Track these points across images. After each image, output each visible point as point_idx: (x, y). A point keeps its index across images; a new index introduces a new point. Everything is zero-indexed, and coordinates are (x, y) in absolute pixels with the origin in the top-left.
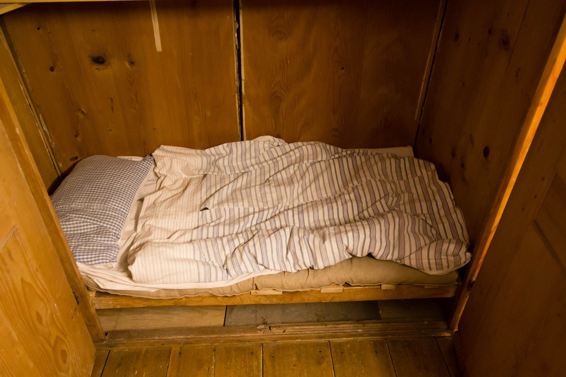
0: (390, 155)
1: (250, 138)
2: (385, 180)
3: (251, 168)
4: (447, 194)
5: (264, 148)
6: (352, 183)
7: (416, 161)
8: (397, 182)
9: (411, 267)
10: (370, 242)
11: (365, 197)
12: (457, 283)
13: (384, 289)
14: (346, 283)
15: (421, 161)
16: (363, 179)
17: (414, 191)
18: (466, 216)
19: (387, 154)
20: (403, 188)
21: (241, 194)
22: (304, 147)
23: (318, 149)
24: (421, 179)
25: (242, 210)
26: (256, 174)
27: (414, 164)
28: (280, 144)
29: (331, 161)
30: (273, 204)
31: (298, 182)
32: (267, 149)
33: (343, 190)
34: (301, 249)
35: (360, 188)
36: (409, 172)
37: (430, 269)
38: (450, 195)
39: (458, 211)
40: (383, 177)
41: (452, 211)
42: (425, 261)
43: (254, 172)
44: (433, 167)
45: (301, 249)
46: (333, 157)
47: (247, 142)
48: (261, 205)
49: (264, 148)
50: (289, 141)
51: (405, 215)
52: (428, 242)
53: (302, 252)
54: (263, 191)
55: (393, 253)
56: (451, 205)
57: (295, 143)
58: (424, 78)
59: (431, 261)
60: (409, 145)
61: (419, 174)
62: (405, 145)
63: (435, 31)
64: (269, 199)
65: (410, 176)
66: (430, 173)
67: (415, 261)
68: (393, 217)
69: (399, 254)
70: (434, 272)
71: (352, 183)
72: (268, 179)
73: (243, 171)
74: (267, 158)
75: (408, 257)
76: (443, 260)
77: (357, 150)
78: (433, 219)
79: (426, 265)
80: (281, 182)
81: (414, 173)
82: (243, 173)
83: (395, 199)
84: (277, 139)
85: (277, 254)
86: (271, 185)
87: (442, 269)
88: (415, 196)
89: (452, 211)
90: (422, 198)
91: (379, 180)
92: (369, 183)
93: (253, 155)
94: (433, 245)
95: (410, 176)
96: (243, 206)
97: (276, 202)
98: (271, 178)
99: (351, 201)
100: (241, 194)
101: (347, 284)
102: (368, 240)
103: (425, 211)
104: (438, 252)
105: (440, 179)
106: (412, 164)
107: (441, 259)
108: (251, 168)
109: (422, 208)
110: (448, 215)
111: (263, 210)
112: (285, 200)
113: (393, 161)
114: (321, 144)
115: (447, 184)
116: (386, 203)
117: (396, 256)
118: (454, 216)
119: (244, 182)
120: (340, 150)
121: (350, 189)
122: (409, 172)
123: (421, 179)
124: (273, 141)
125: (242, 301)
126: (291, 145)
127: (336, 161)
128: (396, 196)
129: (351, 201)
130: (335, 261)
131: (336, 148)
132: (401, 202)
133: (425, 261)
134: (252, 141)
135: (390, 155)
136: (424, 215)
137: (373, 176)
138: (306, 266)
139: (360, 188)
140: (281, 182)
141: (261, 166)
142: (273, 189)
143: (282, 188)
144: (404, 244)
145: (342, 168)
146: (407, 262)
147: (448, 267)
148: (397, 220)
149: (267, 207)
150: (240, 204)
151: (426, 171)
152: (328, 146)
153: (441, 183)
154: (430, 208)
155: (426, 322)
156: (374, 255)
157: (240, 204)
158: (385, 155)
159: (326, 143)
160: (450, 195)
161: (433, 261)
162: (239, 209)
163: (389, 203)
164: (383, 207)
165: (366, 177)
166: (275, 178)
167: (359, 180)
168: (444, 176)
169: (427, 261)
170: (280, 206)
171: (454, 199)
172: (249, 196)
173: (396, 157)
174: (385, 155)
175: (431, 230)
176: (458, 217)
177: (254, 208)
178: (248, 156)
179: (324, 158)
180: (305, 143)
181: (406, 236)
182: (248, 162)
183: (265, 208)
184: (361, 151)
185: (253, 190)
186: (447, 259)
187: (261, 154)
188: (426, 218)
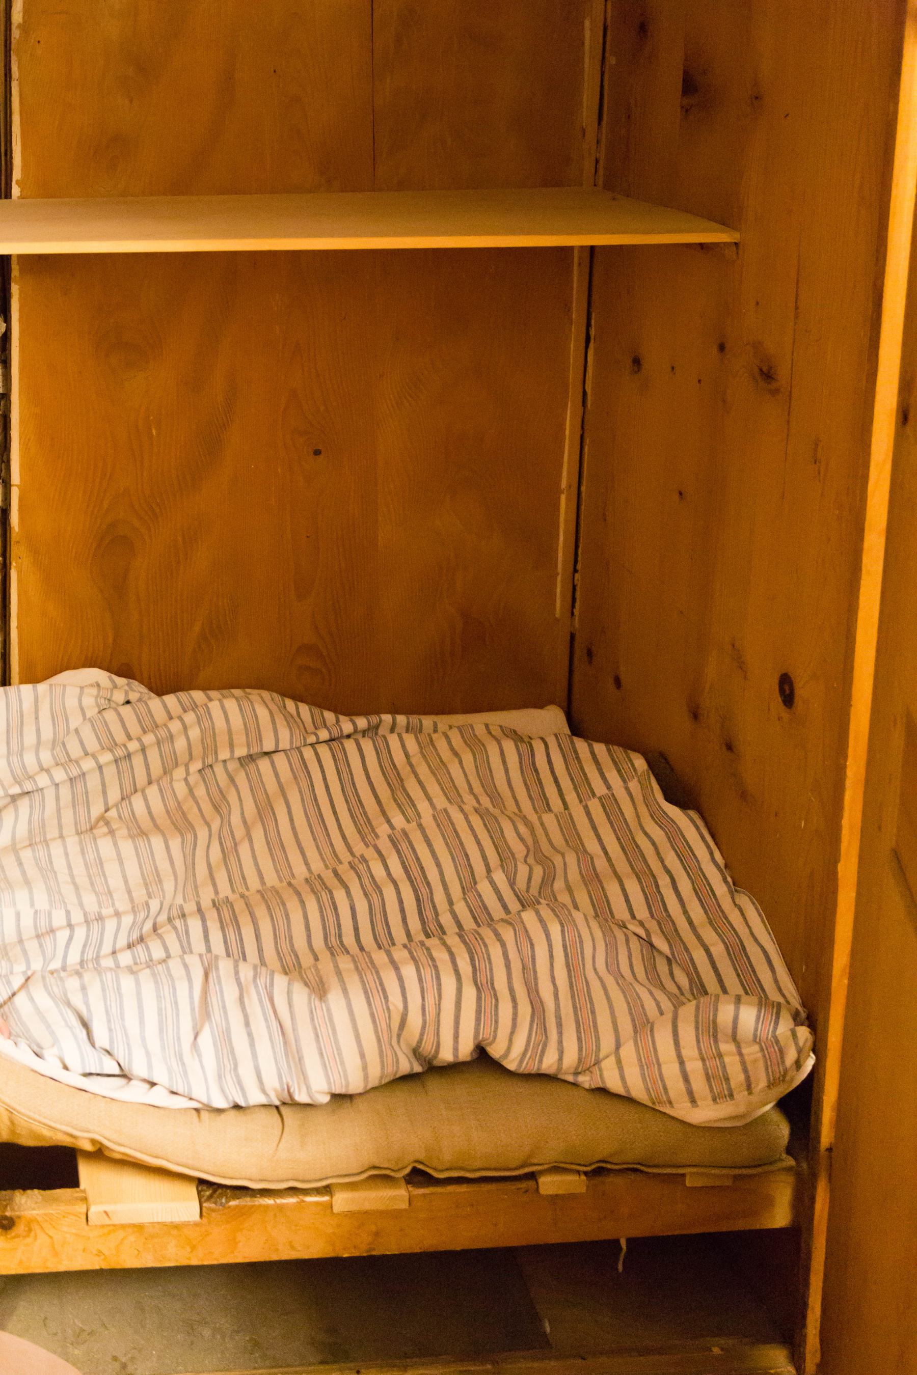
0: (496, 731)
1: (32, 677)
2: (496, 811)
3: (43, 780)
4: (701, 852)
5: (82, 709)
6: (389, 821)
7: (581, 745)
8: (533, 817)
9: (628, 1100)
10: (479, 999)
11: (438, 865)
12: (791, 1162)
13: (551, 1192)
14: (415, 1171)
15: (600, 748)
16: (423, 806)
17: (592, 846)
18: (771, 915)
19: (487, 726)
20: (557, 838)
21: (20, 864)
22: (215, 706)
23: (263, 713)
24: (610, 805)
25: (27, 921)
26: (58, 799)
27: (578, 758)
28: (133, 697)
29: (308, 753)
30: (132, 900)
31: (208, 825)
32: (92, 712)
33: (359, 848)
34: (247, 1024)
35: (416, 837)
36: (566, 783)
37: (693, 1101)
38: (711, 854)
39: (744, 900)
40: (486, 802)
41: (726, 903)
42: (671, 1070)
43: (50, 794)
44: (640, 763)
45: (247, 1024)
46: (312, 739)
47: (27, 688)
48: (90, 902)
49: (82, 709)
50: (160, 691)
51: (578, 916)
52: (666, 1005)
53: (250, 1034)
54: (91, 856)
55: (560, 1042)
56: (721, 890)
57: (182, 695)
58: (564, 484)
59: (689, 1066)
60: (551, 702)
61: (600, 788)
62: (539, 705)
63: (574, 346)
64: (115, 882)
65: (571, 797)
66: (633, 785)
67: (637, 1070)
68: (541, 920)
69: (580, 1049)
70: (705, 1113)
71: (389, 821)
72: (102, 818)
73: (16, 790)
74: (92, 744)
75: (612, 1059)
76: (727, 1060)
77: (387, 718)
78: (672, 935)
79: (676, 1087)
80: (146, 823)
81: (581, 784)
82: (14, 798)
83: (538, 871)
84: (121, 681)
85: (161, 1030)
86: (118, 834)
87: (731, 1095)
88: (601, 864)
89: (726, 903)
90: (622, 866)
91: (476, 810)
92: (443, 820)
93: (47, 733)
94: (687, 1011)
95: (571, 797)
96: (32, 905)
97: (140, 894)
98: (113, 813)
99: (395, 883)
100: (20, 864)
101: (418, 1176)
102: (470, 993)
103: (642, 912)
104: (710, 1030)
105: (668, 799)
106: (572, 758)
107: (720, 1055)
108: (43, 780)
109: (627, 896)
110: (717, 918)
111: (100, 918)
112: (169, 885)
113: (509, 746)
114: (266, 694)
115: (692, 813)
116: (512, 884)
117: (571, 1058)
118: (734, 917)
119: (22, 829)
120: (329, 716)
121: (384, 844)
122: (566, 783)
123: (610, 805)
124: (109, 684)
125: (56, 1254)
126: (170, 699)
127: (324, 750)
128: (539, 862)
129: (395, 883)
130: (366, 1077)
131: (316, 711)
132: (559, 884)
133: (671, 1070)
134: (42, 687)
135: (496, 731)
136: (641, 924)
137: (452, 793)
138: (264, 1092)
139: (416, 837)
140: (146, 823)
141: (75, 772)
142: (127, 847)
143: (157, 842)
144: (593, 1012)
145: (345, 776)
146: (614, 1084)
147: (749, 1087)
148: (555, 929)
149: (111, 911)
150: (22, 896)
151: (623, 780)
152: (290, 704)
153: (673, 811)
154: (654, 898)
155: (716, 1350)
156: (496, 1051)
157: (22, 896)
158: (480, 730)
159: (284, 694)
160: (711, 854)
161: (694, 1066)
162: (18, 915)
163: (521, 883)
164: (500, 898)
165: (429, 799)
166: (126, 813)
167: (410, 812)
168: (680, 793)
169: (677, 1066)
170: (155, 905)
171: (726, 866)
172: (48, 871)
173: (516, 736)
174: (480, 730)
175: (671, 974)
176: (751, 921)
177: (68, 912)
178: (30, 738)
179: (284, 744)
180: (214, 694)
181: (595, 984)
182: (30, 759)
183: (105, 912)
184: (401, 719)
185: (56, 849)
186: (741, 1054)
187: (73, 733)
188: (647, 931)
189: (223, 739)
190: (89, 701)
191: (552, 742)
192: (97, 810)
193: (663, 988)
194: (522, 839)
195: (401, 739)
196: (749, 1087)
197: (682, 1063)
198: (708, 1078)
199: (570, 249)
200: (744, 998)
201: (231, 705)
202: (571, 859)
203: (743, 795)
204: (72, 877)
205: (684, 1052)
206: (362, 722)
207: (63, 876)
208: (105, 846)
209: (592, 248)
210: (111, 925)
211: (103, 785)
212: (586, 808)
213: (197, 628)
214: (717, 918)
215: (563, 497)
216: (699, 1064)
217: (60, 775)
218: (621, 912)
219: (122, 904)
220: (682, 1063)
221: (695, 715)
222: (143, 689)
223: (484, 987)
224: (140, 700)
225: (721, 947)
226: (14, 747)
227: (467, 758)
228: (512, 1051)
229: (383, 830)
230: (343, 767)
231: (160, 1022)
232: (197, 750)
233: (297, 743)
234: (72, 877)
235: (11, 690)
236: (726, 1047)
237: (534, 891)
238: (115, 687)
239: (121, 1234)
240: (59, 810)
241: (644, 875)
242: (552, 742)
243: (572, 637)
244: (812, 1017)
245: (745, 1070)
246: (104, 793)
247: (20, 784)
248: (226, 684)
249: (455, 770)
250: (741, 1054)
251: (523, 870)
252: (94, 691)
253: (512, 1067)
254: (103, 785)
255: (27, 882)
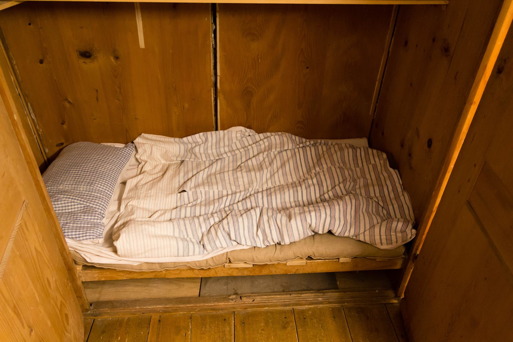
0: (348, 145)
1: (223, 129)
3: (225, 156)
7: (370, 150)
8: (354, 169)
10: (331, 221)
13: (342, 261)
14: (309, 257)
15: (375, 151)
16: (325, 166)
17: (368, 176)
20: (359, 174)
21: (216, 178)
23: (285, 139)
24: (375, 167)
28: (251, 134)
29: (296, 150)
30: (245, 188)
31: (267, 168)
34: (270, 227)
35: (322, 174)
36: (364, 160)
37: (382, 244)
39: (406, 194)
40: (341, 165)
42: (377, 237)
43: (227, 159)
44: (385, 156)
45: (270, 227)
46: (298, 146)
47: (221, 132)
48: (234, 188)
51: (360, 197)
52: (379, 220)
53: (270, 230)
54: (235, 176)
55: (350, 230)
56: (399, 190)
57: (264, 134)
58: (378, 78)
59: (382, 237)
61: (373, 162)
63: (388, 37)
64: (241, 183)
65: (365, 164)
66: (382, 162)
68: (350, 199)
70: (385, 247)
71: (315, 169)
72: (239, 165)
73: (217, 158)
74: (239, 146)
77: (319, 141)
78: (384, 201)
79: (378, 240)
80: (251, 168)
81: (368, 161)
82: (217, 160)
83: (352, 184)
84: (248, 130)
87: (392, 244)
88: (369, 181)
89: (401, 194)
90: (375, 183)
92: (329, 170)
93: (227, 143)
94: (384, 223)
95: (365, 164)
97: (247, 186)
98: (243, 164)
100: (216, 178)
102: (328, 219)
103: (378, 194)
104: (389, 230)
105: (390, 167)
106: (367, 154)
107: (391, 235)
108: (225, 156)
110: (397, 197)
111: (236, 193)
112: (255, 184)
113: (350, 150)
114: (287, 134)
115: (396, 171)
116: (345, 187)
118: (402, 198)
120: (304, 140)
121: (313, 175)
122: (364, 160)
123: (375, 167)
126: (261, 135)
127: (301, 150)
130: (299, 237)
131: (300, 138)
132: (357, 186)
133: (377, 237)
134: (226, 131)
135: (348, 145)
142: (245, 174)
143: (253, 173)
145: (305, 156)
148: (354, 201)
150: (215, 187)
151: (379, 160)
152: (293, 137)
153: (391, 170)
154: (381, 191)
155: (377, 291)
156: (334, 232)
157: (215, 187)
158: (343, 145)
159: (292, 134)
161: (384, 237)
162: (214, 192)
163: (347, 187)
165: (327, 164)
168: (394, 164)
170: (250, 189)
172: (223, 180)
173: (353, 147)
174: (343, 145)
176: (405, 199)
177: (227, 191)
178: (222, 144)
179: (290, 147)
180: (273, 134)
181: (362, 216)
182: (222, 150)
184: (323, 141)
185: (226, 174)
186: (396, 235)
189: (274, 146)
190: (238, 135)
191: (362, 149)
192: (239, 163)
193: (379, 215)
194: (349, 175)
195: (322, 146)
196: (397, 242)
197: (380, 236)
198: (386, 240)
199: (393, 5)
200: (400, 220)
201: (277, 137)
202: (362, 180)
203: (411, 168)
204: (230, 181)
205: (381, 234)
206: (312, 142)
207: (227, 182)
208: (239, 174)
209: (400, 5)
210: (238, 195)
211: (241, 156)
212: (368, 167)
213: (270, 116)
214: (397, 197)
215: (377, 82)
216: (385, 237)
217: (229, 154)
218: (372, 194)
219: (242, 188)
220: (380, 236)
221: (402, 146)
222: (254, 132)
223: (332, 217)
224: (253, 135)
225: (397, 205)
226: (218, 146)
227: (339, 153)
228: (337, 230)
229: (313, 171)
230: (305, 156)
231: (248, 229)
232: (267, 149)
233: (294, 147)
234: (230, 181)
235: (217, 132)
236: (393, 233)
237: (350, 189)
238: (246, 131)
239: (233, 270)
240: (229, 163)
241: (380, 185)
242: (362, 149)
243: (373, 120)
244: (416, 226)
245: (397, 238)
246: (241, 159)
247: (218, 156)
248: (276, 131)
249: (335, 156)
250: (396, 235)
251: (348, 183)
252: (240, 133)
253: (336, 235)
254: (241, 156)
255: (217, 183)
